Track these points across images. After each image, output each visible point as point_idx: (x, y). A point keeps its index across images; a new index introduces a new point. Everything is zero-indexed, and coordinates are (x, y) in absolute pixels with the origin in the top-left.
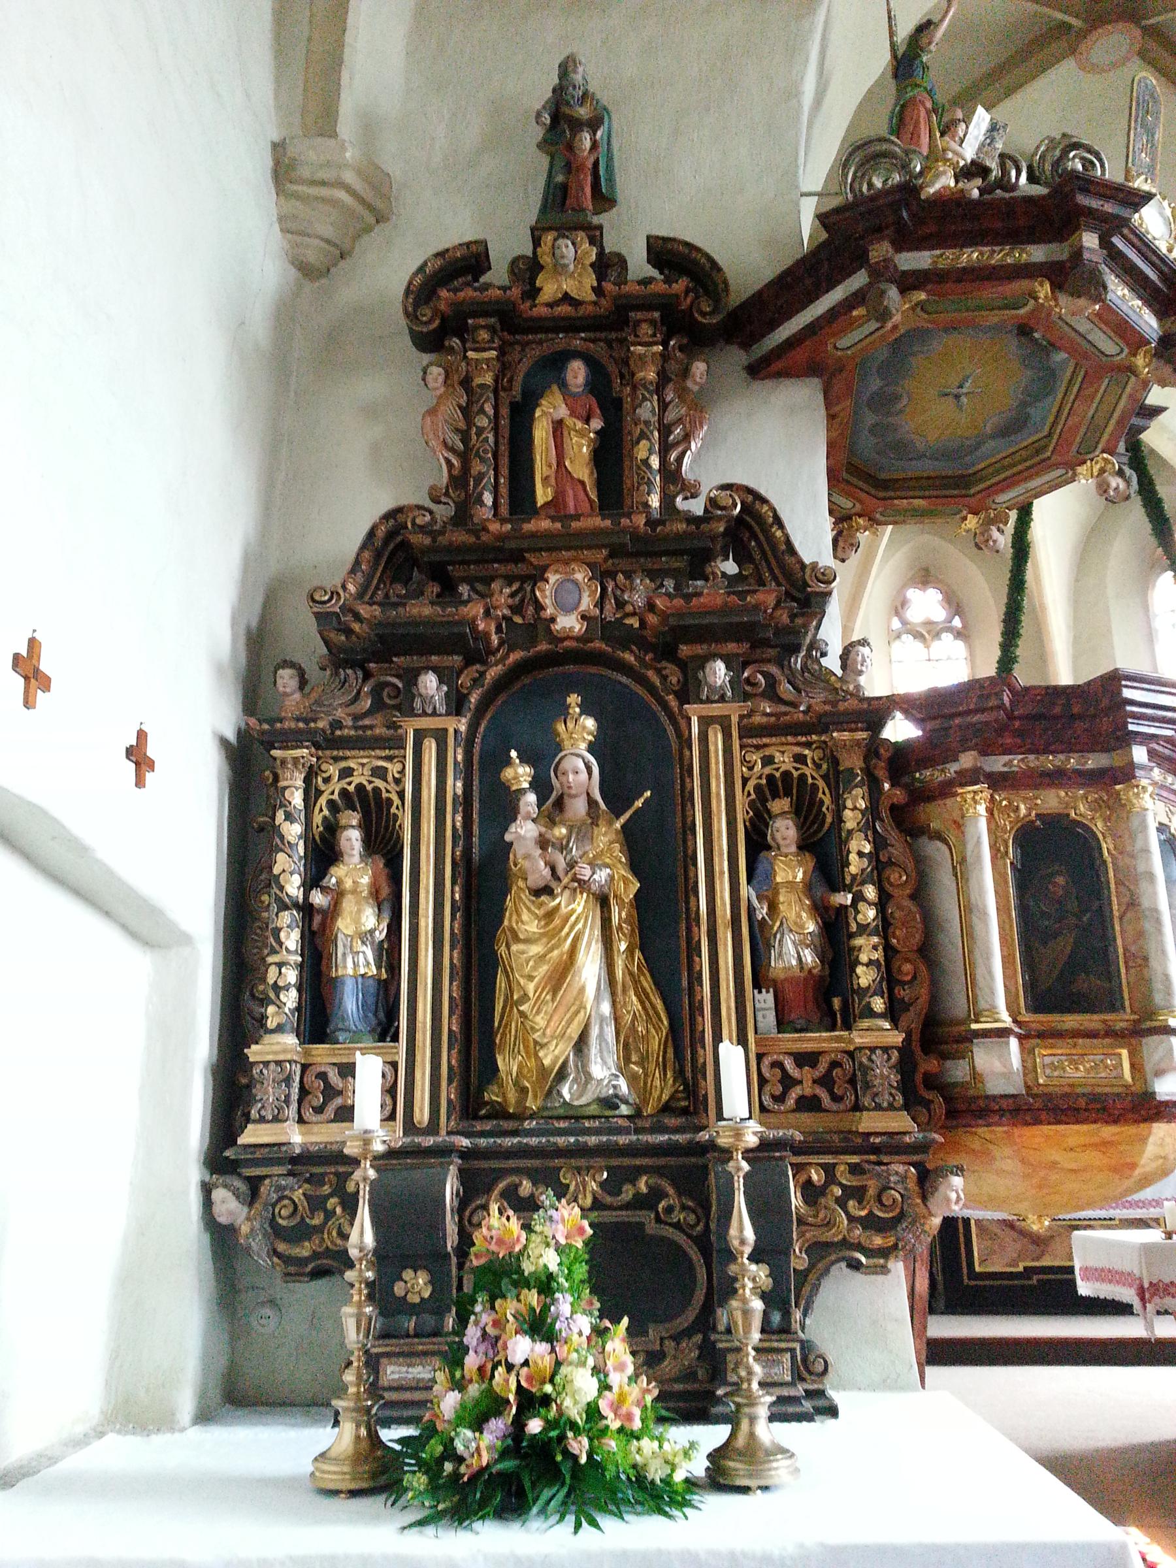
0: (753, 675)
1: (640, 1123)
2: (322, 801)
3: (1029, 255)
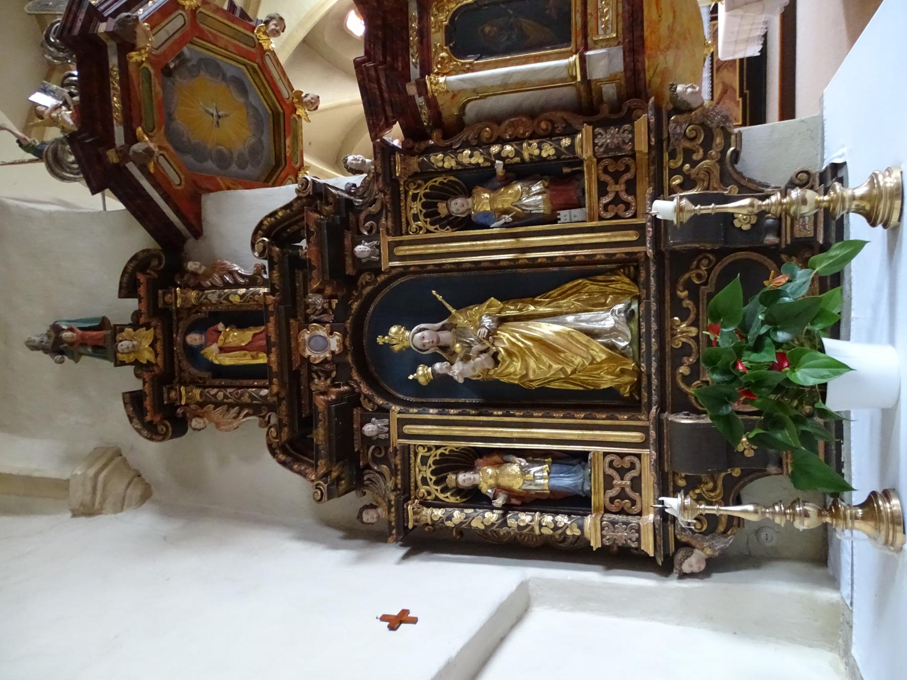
0: (365, 228)
1: (644, 296)
2: (441, 496)
3: (114, 66)
